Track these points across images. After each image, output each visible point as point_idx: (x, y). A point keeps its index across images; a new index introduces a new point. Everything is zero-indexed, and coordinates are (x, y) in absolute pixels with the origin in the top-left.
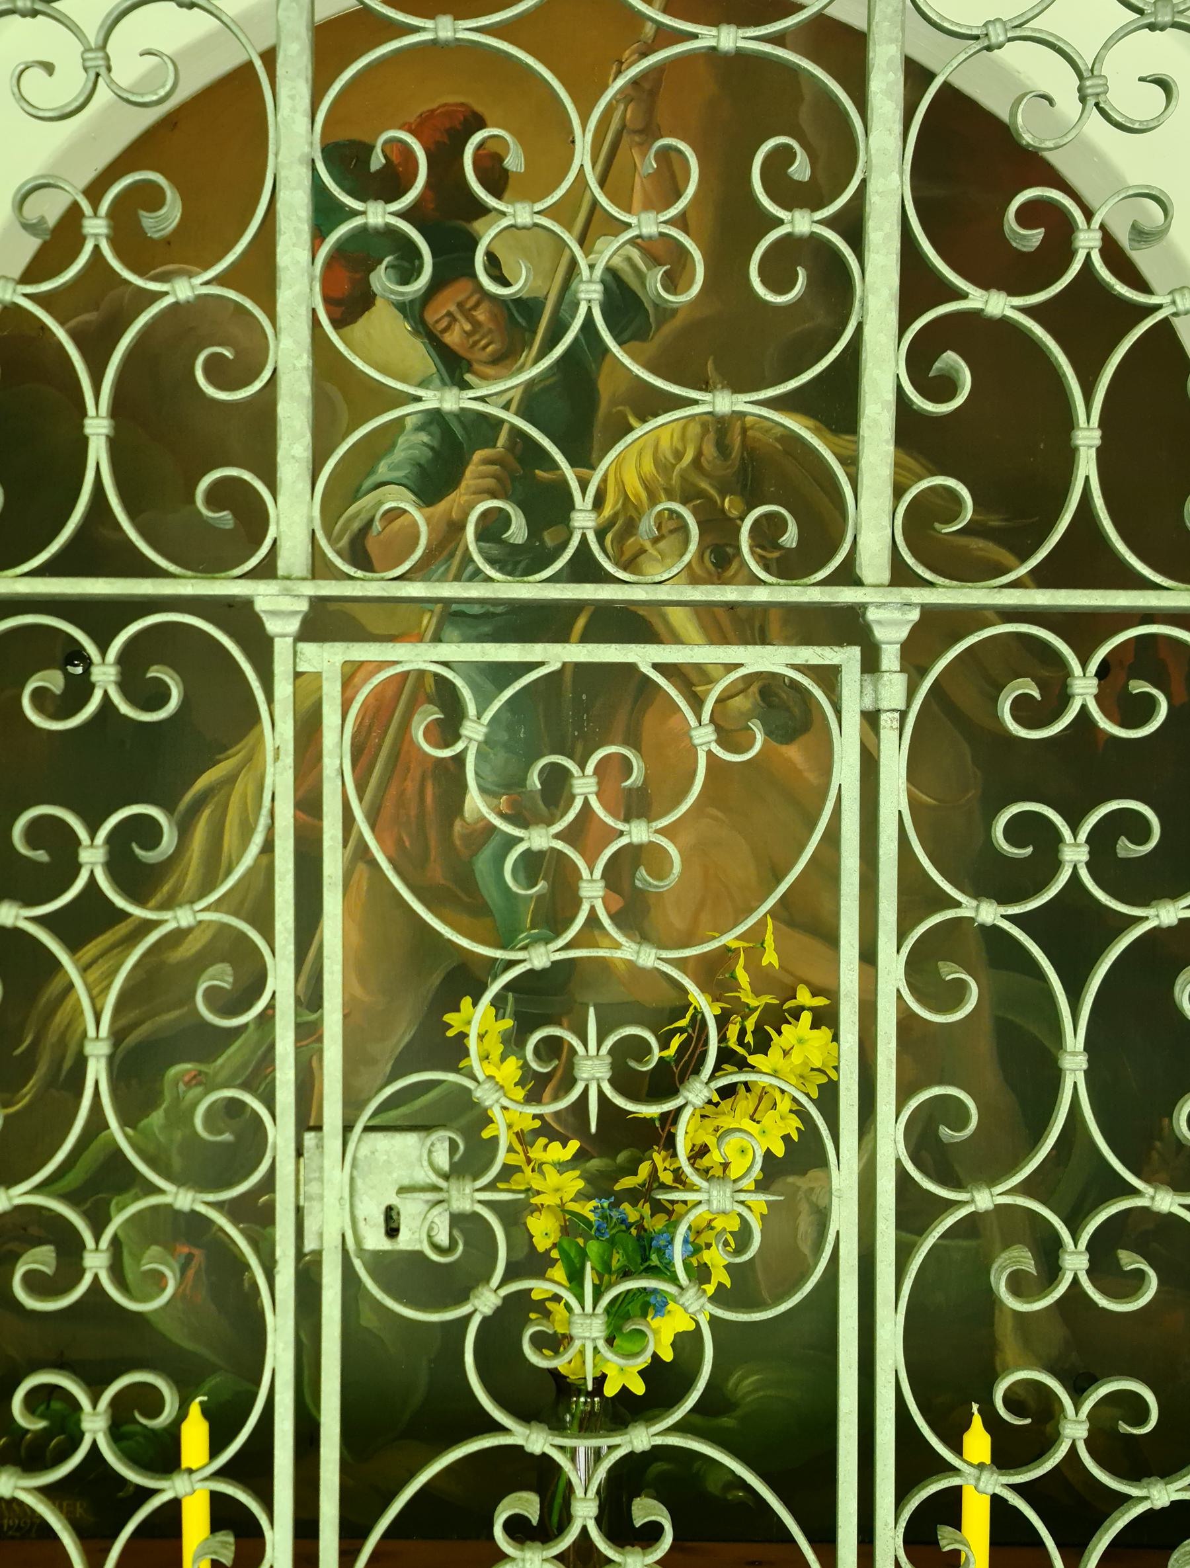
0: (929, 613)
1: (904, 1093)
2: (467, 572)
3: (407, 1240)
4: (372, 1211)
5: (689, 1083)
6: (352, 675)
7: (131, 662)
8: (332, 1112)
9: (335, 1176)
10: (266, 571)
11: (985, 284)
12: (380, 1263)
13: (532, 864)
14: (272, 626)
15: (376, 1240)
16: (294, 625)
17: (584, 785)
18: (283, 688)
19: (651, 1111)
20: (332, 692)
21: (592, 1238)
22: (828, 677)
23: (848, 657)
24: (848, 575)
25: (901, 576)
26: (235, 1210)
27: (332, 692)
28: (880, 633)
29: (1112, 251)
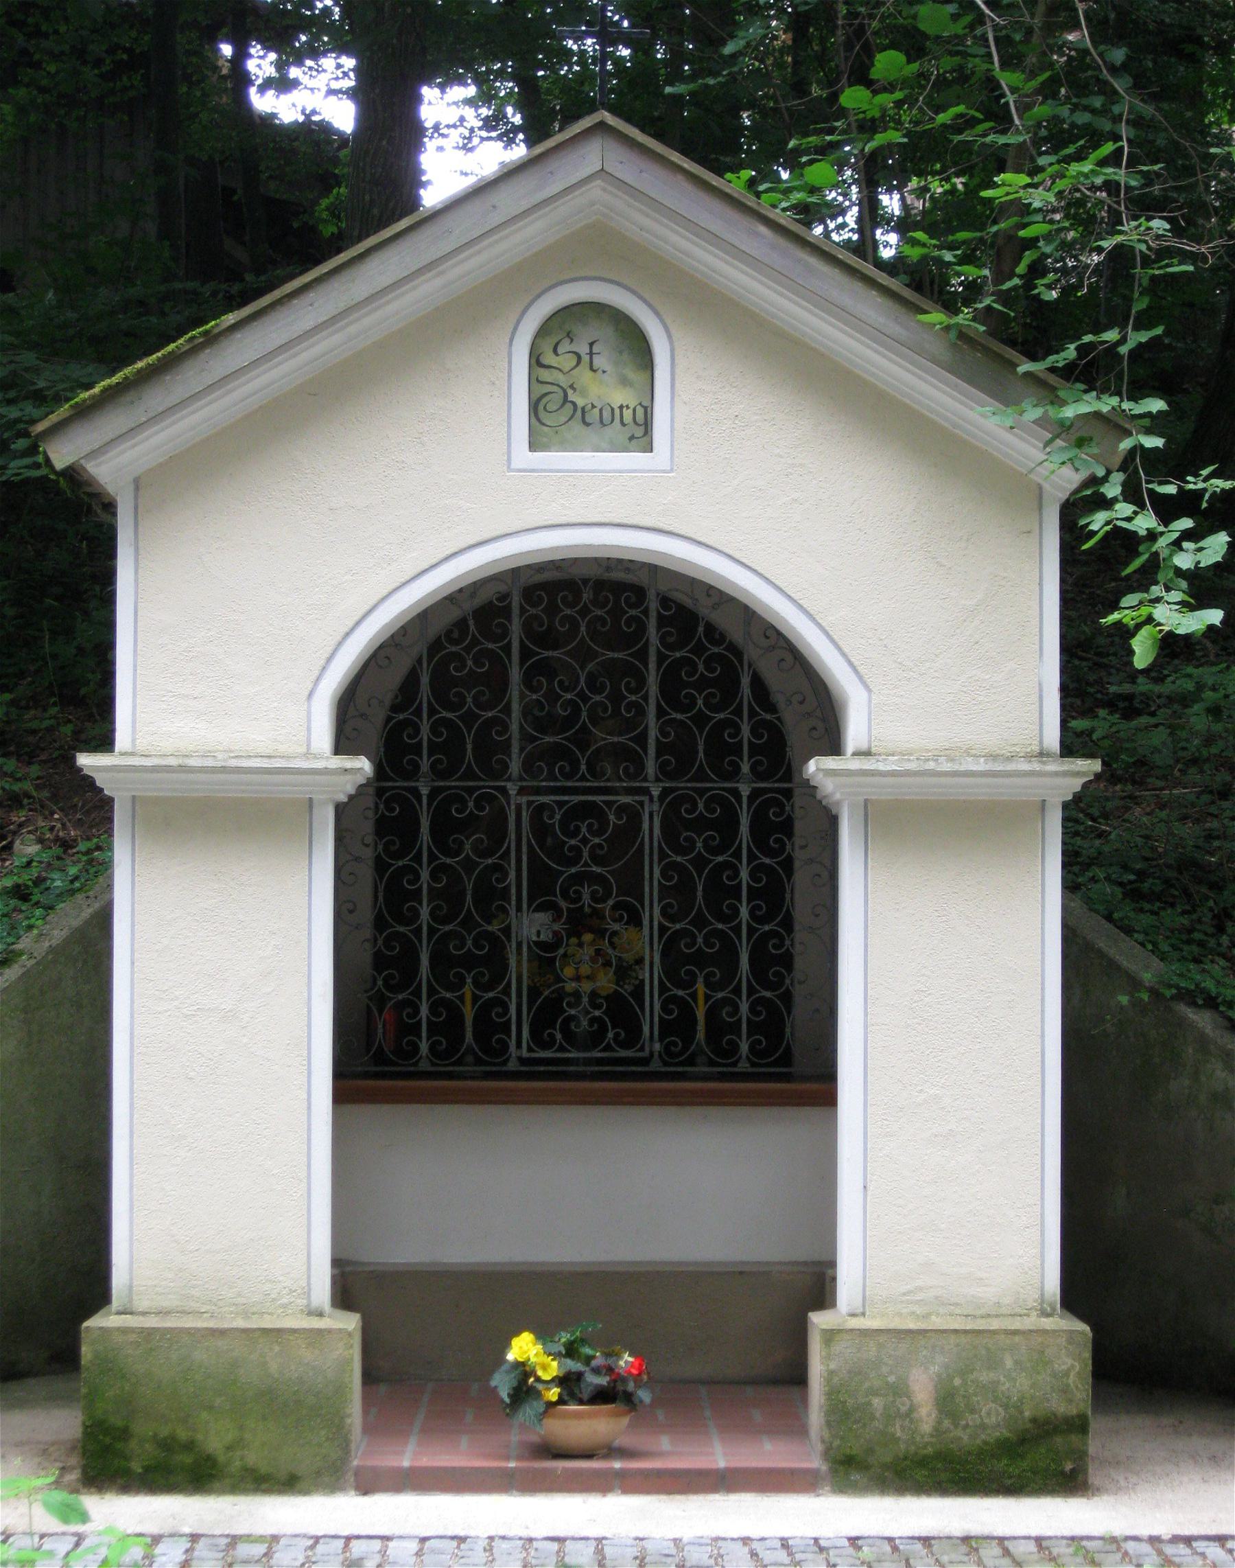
0: (664, 789)
1: (660, 901)
2: (556, 779)
3: (542, 937)
4: (534, 931)
5: (825, 797)
6: (529, 803)
7: (477, 801)
8: (525, 906)
9: (526, 922)
10: (509, 779)
11: (676, 711)
12: (536, 943)
13: (571, 848)
14: (511, 792)
15: (535, 938)
16: (515, 792)
17: (584, 830)
18: (513, 807)
19: (783, 950)
20: (524, 807)
21: (834, 97)
22: (641, 804)
23: (646, 799)
24: (645, 780)
25: (658, 780)
26: (757, 858)
27: (524, 807)
28: (653, 793)
29: (565, 955)
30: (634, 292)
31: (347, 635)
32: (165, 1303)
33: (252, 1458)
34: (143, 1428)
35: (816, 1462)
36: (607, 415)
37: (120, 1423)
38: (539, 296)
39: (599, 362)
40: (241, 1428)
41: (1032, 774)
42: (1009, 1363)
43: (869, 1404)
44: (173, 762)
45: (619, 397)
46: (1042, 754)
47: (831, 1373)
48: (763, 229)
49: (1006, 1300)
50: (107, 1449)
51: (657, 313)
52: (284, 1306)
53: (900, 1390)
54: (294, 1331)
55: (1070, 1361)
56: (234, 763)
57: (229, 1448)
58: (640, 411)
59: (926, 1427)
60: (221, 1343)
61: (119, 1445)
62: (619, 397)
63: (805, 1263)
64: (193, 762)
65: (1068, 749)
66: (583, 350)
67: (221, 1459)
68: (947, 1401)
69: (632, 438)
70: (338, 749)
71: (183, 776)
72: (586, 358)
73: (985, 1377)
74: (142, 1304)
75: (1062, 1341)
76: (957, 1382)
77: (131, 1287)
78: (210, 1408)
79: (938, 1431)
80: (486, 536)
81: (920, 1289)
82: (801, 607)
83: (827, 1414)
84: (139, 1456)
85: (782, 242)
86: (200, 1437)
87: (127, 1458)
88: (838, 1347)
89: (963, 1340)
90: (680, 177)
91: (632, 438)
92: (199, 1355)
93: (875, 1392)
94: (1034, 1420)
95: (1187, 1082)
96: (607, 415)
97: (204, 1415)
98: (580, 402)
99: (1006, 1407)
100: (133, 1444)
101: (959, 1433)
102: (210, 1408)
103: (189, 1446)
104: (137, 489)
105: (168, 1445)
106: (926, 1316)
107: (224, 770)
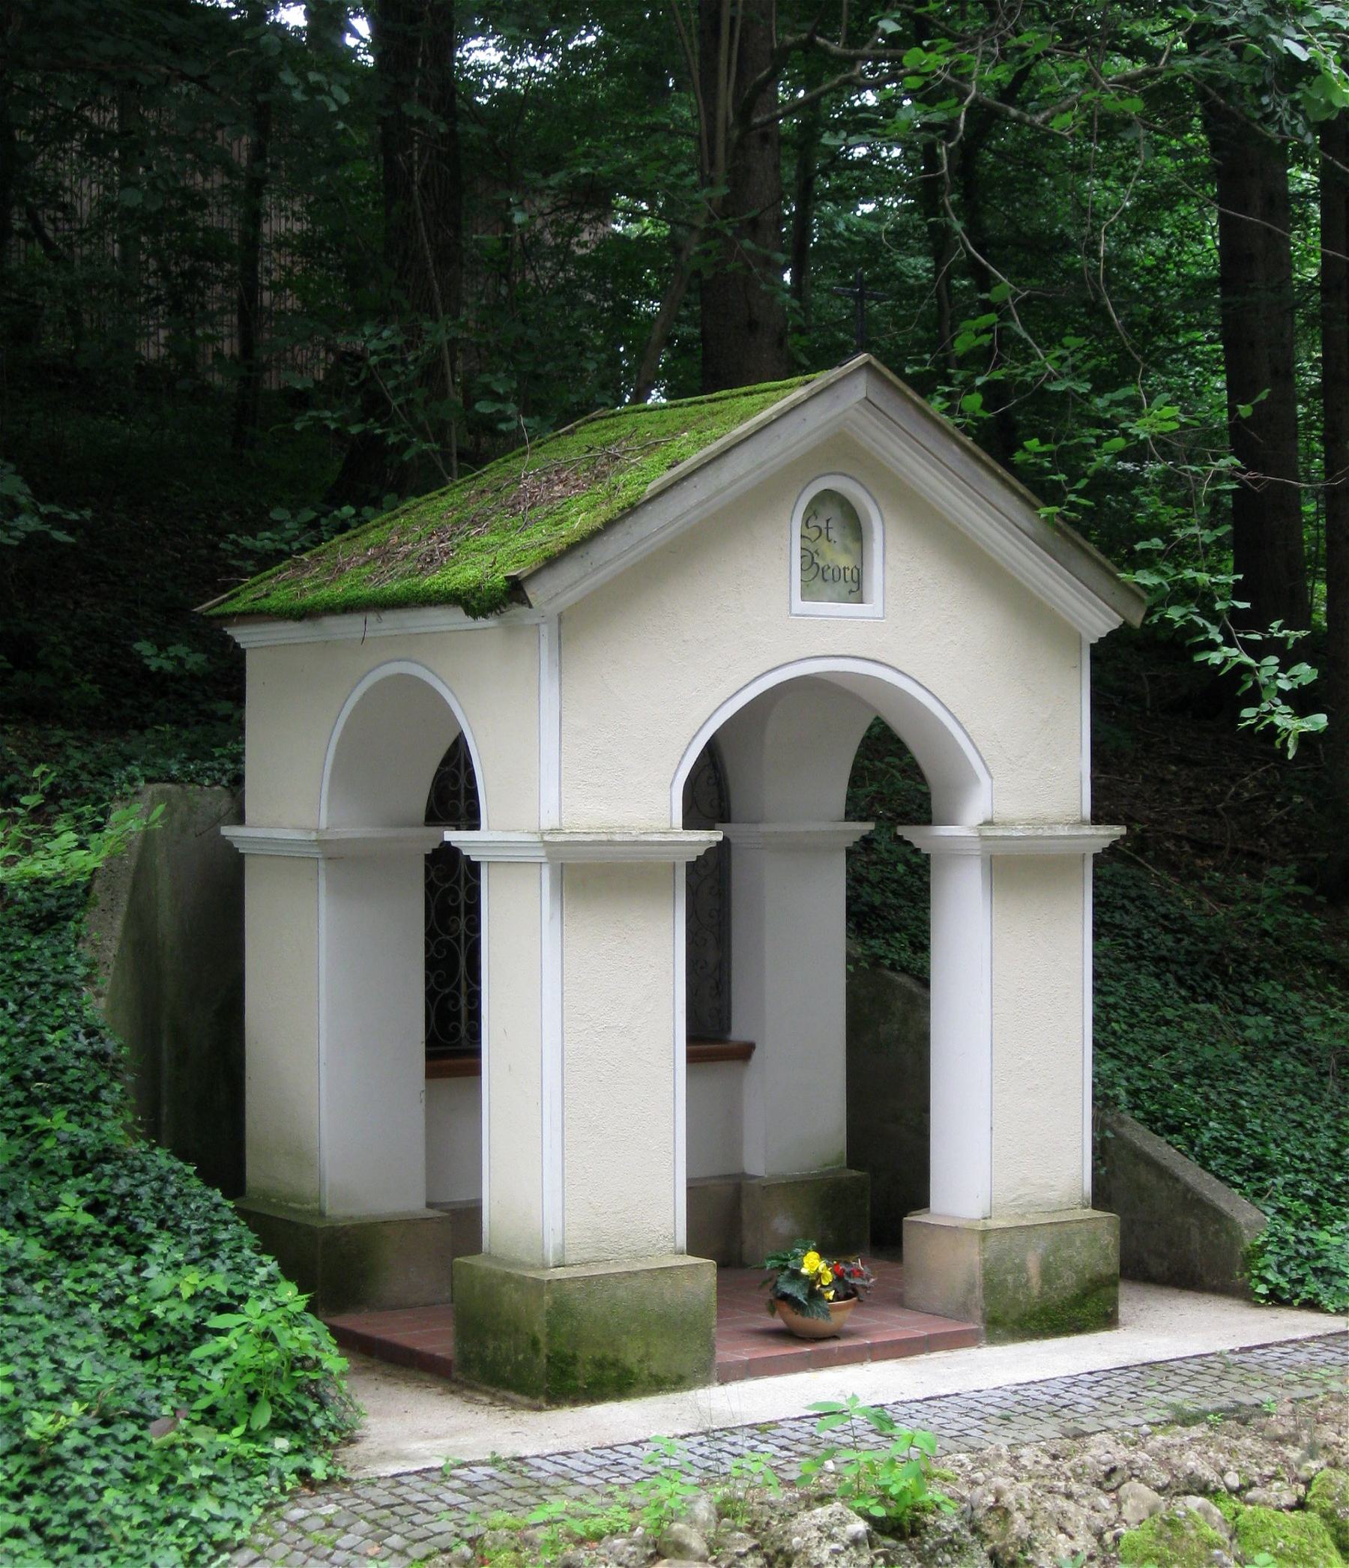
30: (862, 485)
31: (694, 737)
32: (586, 1256)
33: (656, 1367)
34: (585, 1354)
35: (976, 1325)
36: (836, 573)
37: (570, 1352)
38: (810, 483)
39: (832, 534)
40: (648, 1345)
41: (1092, 836)
42: (1078, 1244)
43: (1005, 1280)
44: (604, 838)
45: (844, 561)
46: (1083, 822)
47: (986, 1260)
48: (955, 448)
49: (1065, 1200)
50: (563, 1373)
51: (875, 501)
52: (660, 1249)
53: (1021, 1268)
54: (681, 1267)
55: (1109, 1238)
56: (643, 838)
57: (641, 1361)
58: (855, 572)
59: (1035, 1292)
60: (635, 1282)
61: (571, 1368)
62: (844, 561)
63: (720, 1177)
64: (618, 838)
65: (1096, 819)
66: (823, 525)
67: (636, 1370)
68: (1047, 1273)
69: (851, 592)
70: (688, 825)
71: (611, 848)
72: (824, 531)
73: (1065, 1253)
74: (571, 1258)
75: (1105, 1224)
76: (1051, 1259)
77: (563, 1247)
78: (628, 1332)
79: (1042, 1294)
80: (778, 664)
81: (1020, 1196)
82: (955, 718)
83: (984, 1289)
84: (584, 1373)
85: (967, 459)
86: (621, 1356)
87: (575, 1379)
88: (992, 1241)
89: (1055, 1229)
90: (910, 406)
91: (851, 592)
92: (621, 1293)
93: (1007, 1272)
94: (1090, 1280)
95: (896, 1026)
96: (836, 573)
97: (624, 1338)
98: (821, 564)
99: (1076, 1272)
100: (579, 1366)
101: (1052, 1294)
102: (628, 1332)
103: (614, 1364)
104: (560, 621)
105: (600, 1364)
106: (1023, 1216)
107: (635, 843)
